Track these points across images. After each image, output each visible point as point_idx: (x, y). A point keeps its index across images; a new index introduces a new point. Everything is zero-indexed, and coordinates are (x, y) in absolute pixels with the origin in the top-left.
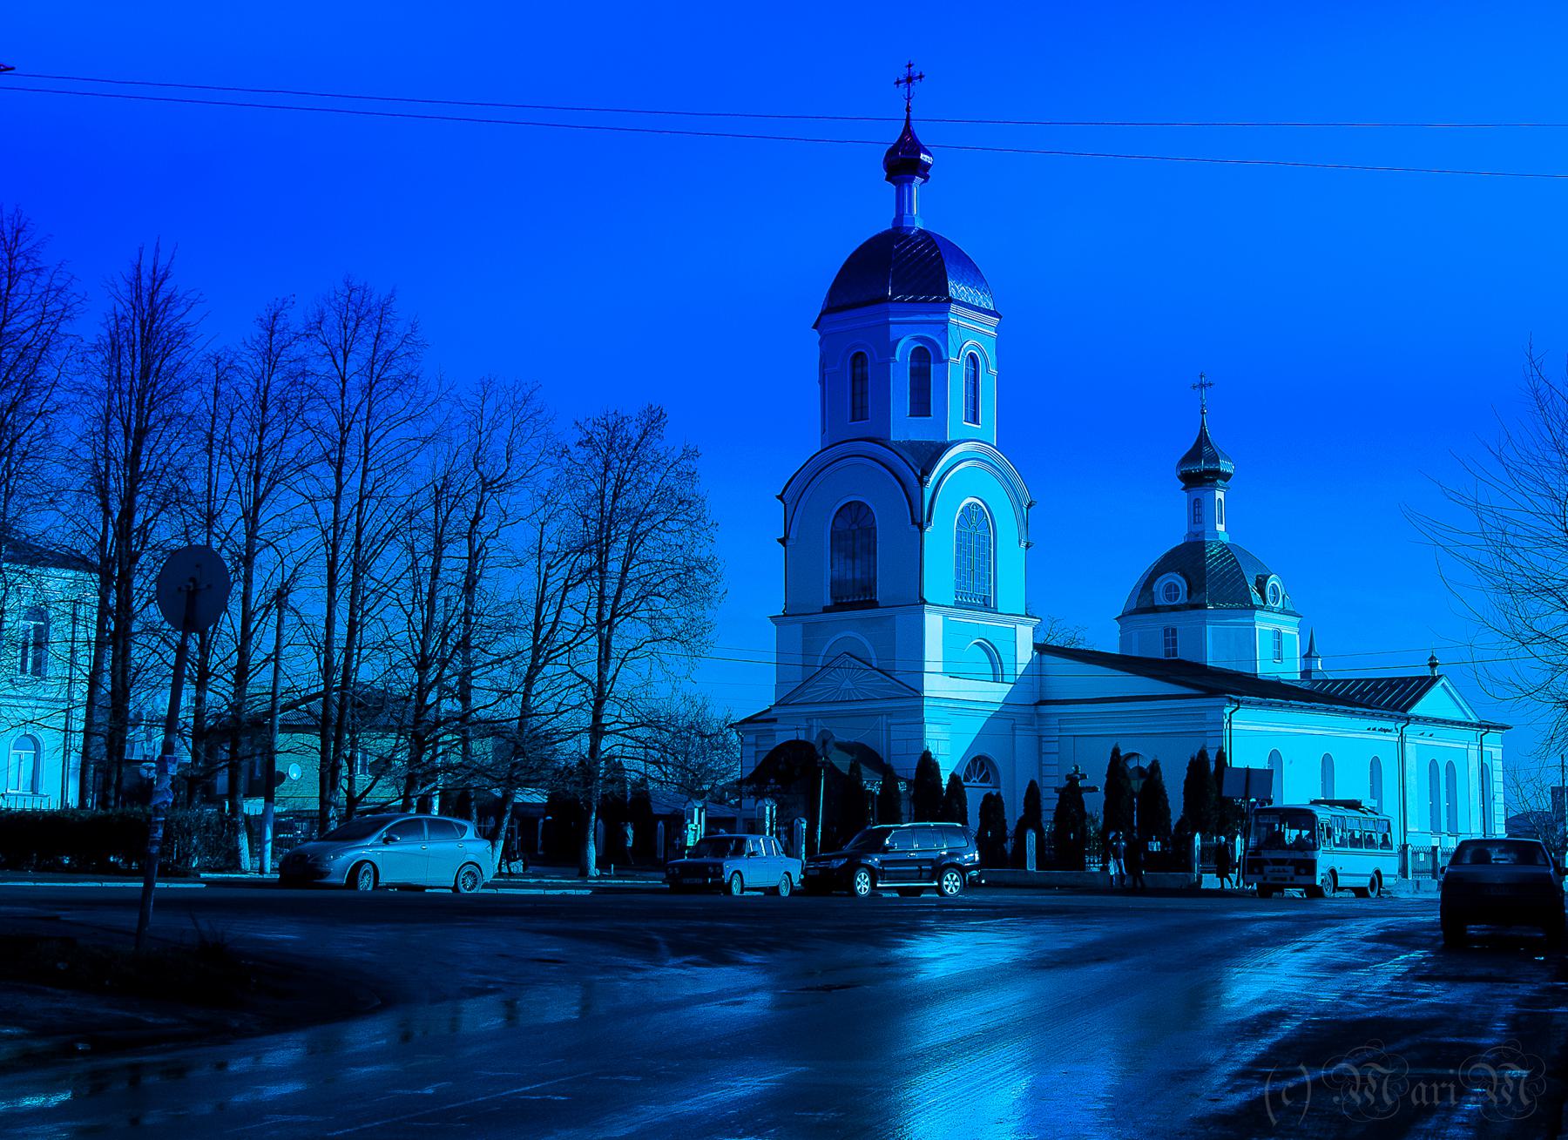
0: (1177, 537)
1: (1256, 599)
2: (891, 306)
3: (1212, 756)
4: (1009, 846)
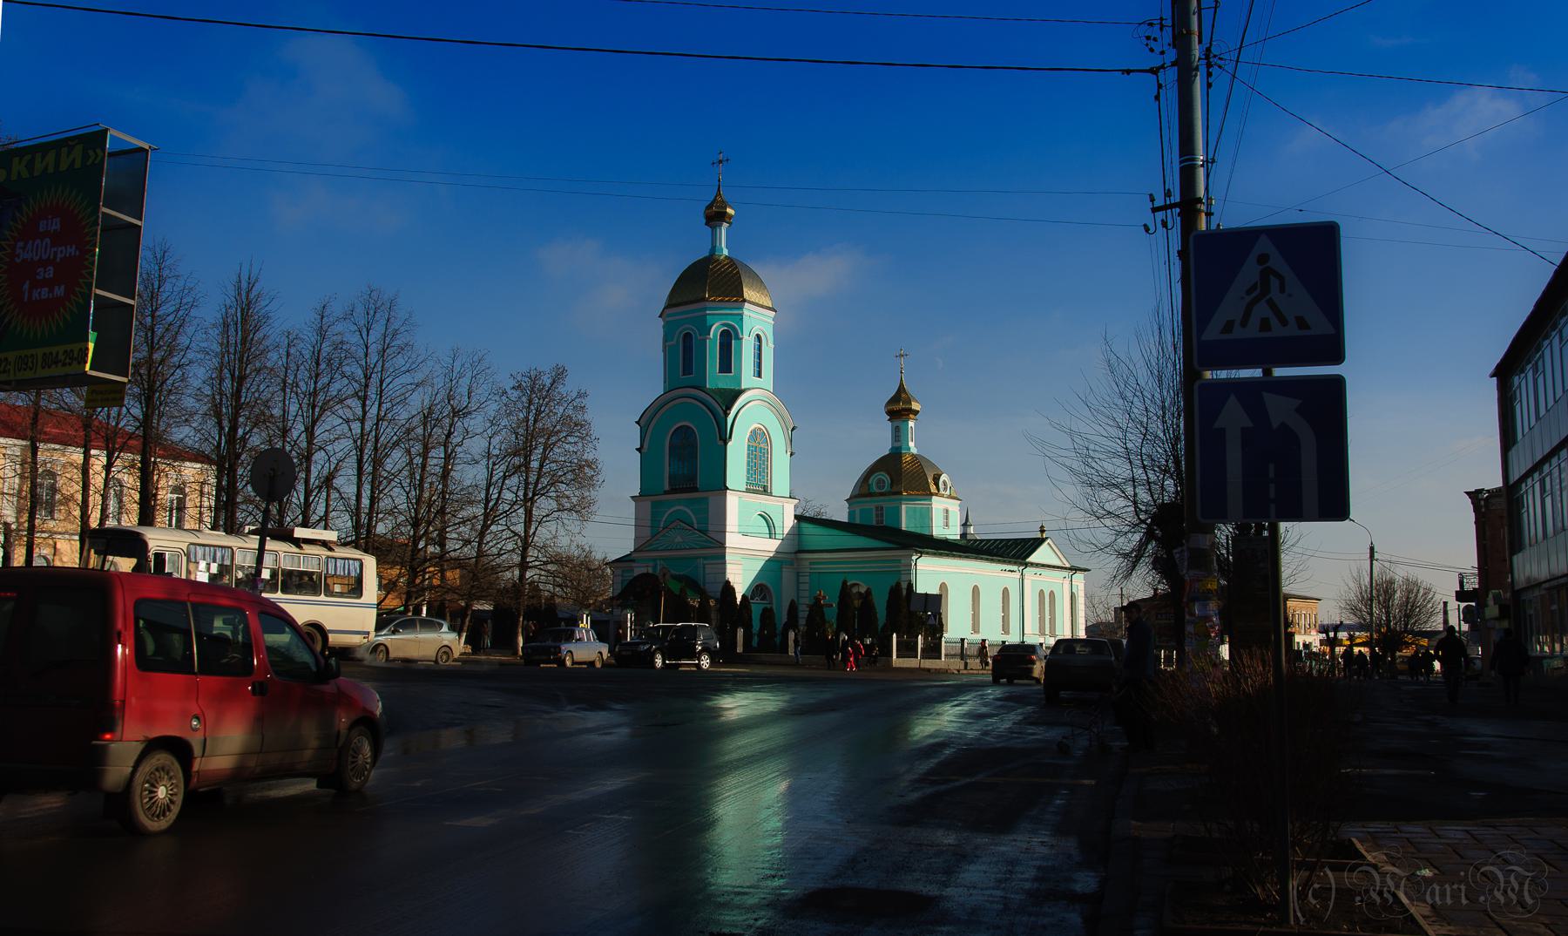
0: (882, 446)
1: (933, 489)
3: (904, 585)
4: (778, 640)
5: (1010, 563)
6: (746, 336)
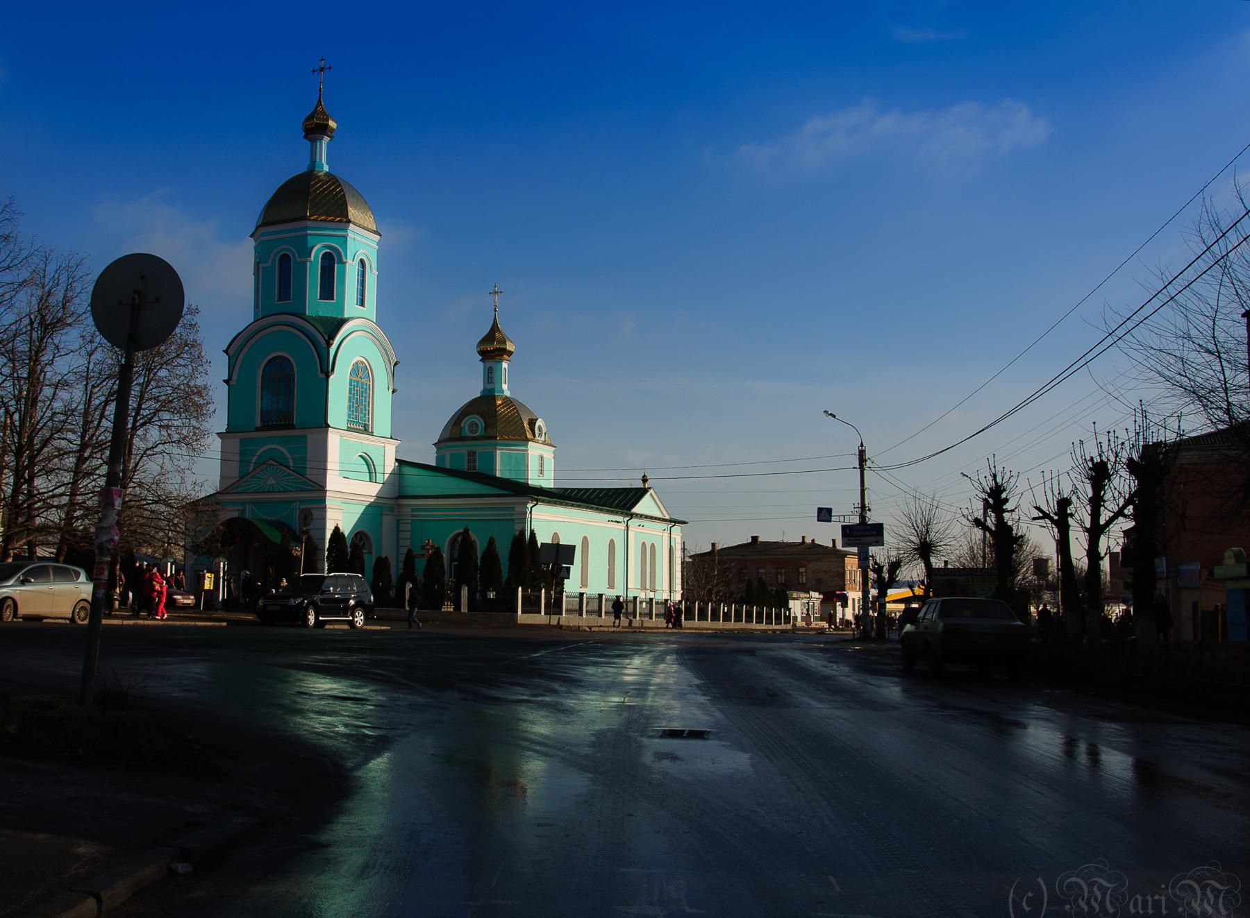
1: (529, 436)
2: (309, 224)
4: (392, 593)
5: (617, 513)
6: (349, 260)
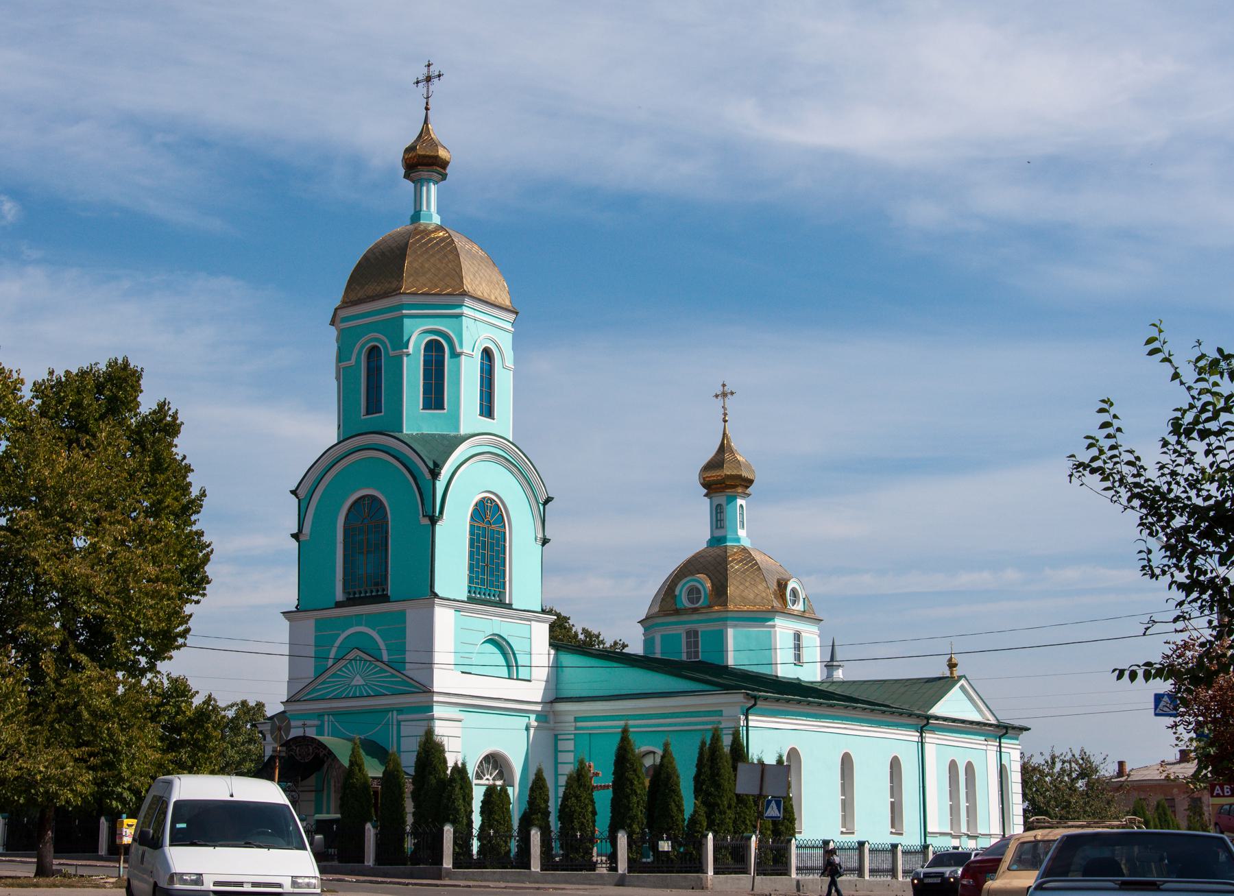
0: (690, 532)
3: (727, 741)
